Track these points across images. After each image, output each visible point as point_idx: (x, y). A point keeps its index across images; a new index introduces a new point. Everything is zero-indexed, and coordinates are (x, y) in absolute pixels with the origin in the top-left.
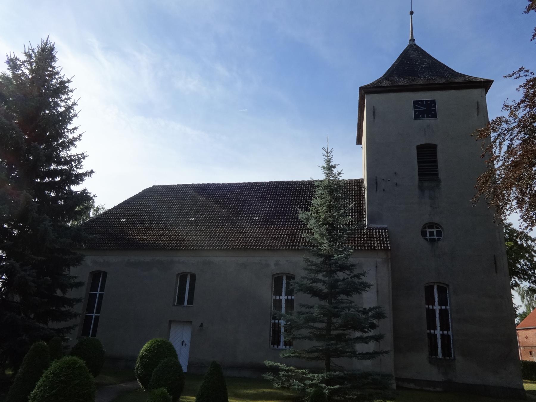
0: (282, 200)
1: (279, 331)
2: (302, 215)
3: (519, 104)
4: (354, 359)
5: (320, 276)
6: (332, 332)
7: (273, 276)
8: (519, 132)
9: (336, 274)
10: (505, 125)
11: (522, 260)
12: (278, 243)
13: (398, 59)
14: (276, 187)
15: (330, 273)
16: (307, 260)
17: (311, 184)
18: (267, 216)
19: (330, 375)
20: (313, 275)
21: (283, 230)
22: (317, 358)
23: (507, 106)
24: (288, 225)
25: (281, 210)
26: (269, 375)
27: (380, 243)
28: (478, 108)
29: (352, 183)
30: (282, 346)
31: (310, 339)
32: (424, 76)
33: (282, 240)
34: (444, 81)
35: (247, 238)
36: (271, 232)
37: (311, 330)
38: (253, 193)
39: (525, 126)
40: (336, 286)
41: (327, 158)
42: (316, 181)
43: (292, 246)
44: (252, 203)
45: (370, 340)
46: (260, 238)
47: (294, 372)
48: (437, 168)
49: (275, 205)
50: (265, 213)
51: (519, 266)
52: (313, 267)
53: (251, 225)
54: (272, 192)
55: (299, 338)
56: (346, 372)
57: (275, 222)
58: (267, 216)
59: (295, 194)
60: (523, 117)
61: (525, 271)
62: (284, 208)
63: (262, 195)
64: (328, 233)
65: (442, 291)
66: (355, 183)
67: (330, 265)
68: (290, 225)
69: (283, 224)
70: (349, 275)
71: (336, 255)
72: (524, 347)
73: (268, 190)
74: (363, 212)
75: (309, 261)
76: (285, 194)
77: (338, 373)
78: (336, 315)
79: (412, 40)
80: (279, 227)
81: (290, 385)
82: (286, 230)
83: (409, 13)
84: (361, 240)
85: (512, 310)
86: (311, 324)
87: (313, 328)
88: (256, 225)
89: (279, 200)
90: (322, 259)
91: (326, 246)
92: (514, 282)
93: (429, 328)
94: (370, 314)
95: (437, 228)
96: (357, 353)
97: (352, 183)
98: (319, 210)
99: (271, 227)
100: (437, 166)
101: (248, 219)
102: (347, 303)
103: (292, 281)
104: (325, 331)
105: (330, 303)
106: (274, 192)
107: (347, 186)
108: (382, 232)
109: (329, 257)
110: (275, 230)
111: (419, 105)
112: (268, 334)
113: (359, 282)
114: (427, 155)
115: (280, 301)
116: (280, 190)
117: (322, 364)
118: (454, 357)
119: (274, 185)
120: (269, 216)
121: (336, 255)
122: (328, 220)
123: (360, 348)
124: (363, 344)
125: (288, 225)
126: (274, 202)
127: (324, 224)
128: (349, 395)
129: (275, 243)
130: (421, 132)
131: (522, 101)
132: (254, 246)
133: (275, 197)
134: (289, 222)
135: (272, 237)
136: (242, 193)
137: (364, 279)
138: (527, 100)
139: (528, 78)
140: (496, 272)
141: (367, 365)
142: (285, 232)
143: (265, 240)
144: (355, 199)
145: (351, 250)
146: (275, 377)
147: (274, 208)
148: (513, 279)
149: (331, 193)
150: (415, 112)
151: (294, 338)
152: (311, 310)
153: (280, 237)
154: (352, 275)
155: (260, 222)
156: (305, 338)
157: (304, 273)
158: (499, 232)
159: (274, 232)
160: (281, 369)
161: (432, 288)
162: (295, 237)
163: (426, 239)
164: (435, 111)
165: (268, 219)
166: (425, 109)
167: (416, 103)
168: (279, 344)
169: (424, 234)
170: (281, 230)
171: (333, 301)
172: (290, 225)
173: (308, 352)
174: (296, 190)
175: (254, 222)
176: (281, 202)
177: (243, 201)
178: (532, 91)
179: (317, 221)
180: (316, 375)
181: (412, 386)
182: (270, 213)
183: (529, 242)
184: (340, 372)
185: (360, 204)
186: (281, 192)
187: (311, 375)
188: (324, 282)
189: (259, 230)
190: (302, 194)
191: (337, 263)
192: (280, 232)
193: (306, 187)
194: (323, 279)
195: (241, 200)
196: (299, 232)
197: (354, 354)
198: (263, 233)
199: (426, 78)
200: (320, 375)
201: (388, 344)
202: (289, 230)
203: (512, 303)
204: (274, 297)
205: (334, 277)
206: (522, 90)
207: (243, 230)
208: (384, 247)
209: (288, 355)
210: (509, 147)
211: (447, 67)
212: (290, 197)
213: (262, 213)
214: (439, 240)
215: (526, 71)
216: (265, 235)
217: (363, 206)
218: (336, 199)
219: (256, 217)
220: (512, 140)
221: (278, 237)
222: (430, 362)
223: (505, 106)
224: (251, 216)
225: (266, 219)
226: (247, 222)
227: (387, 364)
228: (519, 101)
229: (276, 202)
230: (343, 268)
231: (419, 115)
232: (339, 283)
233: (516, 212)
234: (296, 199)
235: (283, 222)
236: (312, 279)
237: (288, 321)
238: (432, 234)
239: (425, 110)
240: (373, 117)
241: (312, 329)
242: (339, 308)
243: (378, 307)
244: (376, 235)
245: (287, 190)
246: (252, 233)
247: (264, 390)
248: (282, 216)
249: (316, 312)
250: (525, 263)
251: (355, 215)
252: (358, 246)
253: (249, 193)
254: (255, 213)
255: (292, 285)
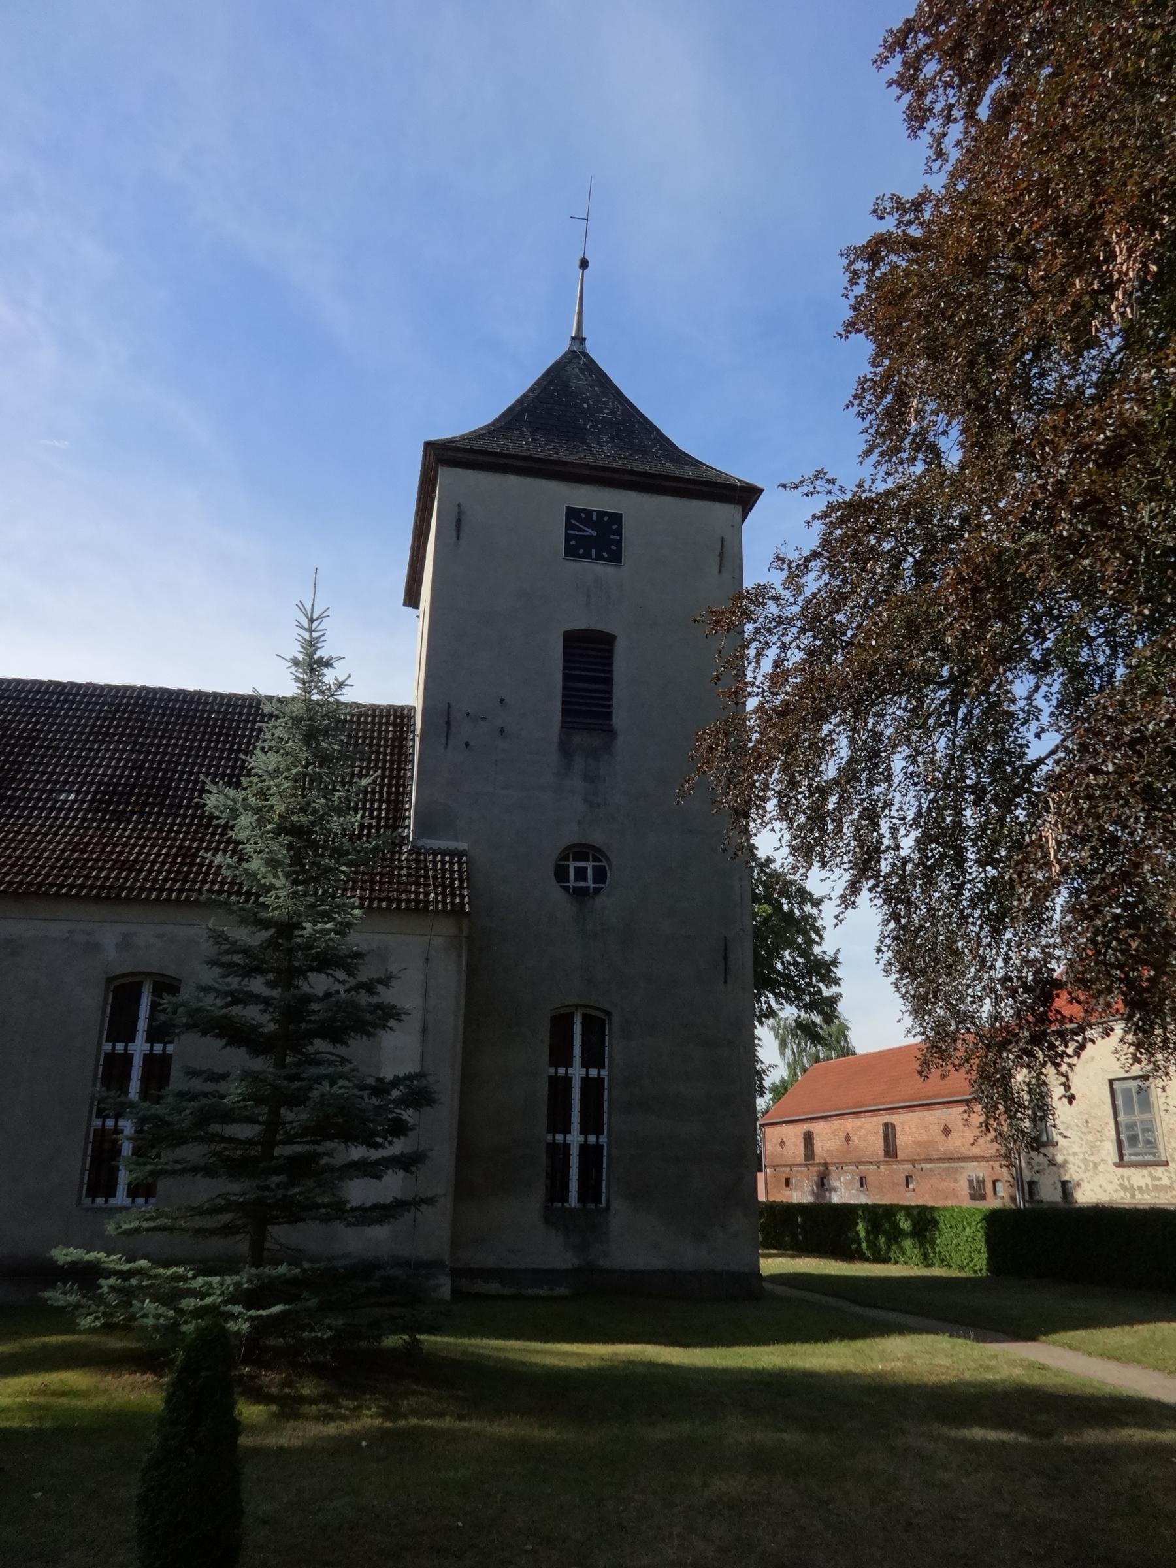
0: (159, 746)
1: (116, 1151)
2: (216, 799)
3: (807, 560)
4: (339, 1226)
5: (257, 985)
6: (278, 1151)
7: (109, 981)
8: (803, 630)
9: (306, 978)
10: (773, 608)
11: (787, 952)
12: (136, 880)
13: (537, 383)
14: (143, 705)
15: (287, 976)
16: (218, 937)
17: (250, 706)
18: (104, 793)
19: (259, 1277)
20: (234, 982)
21: (156, 839)
22: (227, 1230)
23: (783, 560)
24: (173, 824)
25: (155, 778)
26: (65, 1293)
27: (443, 893)
28: (721, 554)
29: (381, 716)
30: (121, 1198)
31: (209, 1171)
32: (600, 444)
33: (150, 871)
34: (647, 468)
35: (29, 858)
36: (115, 845)
37: (218, 1148)
38: (66, 716)
39: (816, 617)
40: (300, 1011)
41: (307, 635)
42: (270, 699)
43: (181, 891)
44: (57, 748)
45: (387, 1168)
46: (77, 860)
47: (150, 1277)
48: (611, 699)
49: (136, 761)
50: (100, 783)
51: (779, 966)
52: (237, 958)
53: (47, 818)
54: (129, 719)
55: (174, 1173)
56: (306, 1265)
57: (133, 813)
58: (104, 793)
59: (204, 733)
60: (814, 595)
61: (791, 978)
62: (166, 771)
63: (94, 726)
64: (292, 857)
65: (595, 1027)
66: (388, 716)
67: (290, 952)
68: (181, 825)
69: (155, 823)
70: (343, 982)
71: (308, 925)
72: (774, 1167)
73: (117, 711)
74: (403, 802)
75: (227, 939)
76: (173, 731)
77: (283, 1269)
78: (296, 1100)
79: (579, 339)
80: (143, 830)
81: (132, 1317)
82: (165, 839)
83: (578, 263)
84: (390, 883)
85: (752, 1076)
86: (216, 1128)
87: (222, 1139)
88: (65, 819)
89: (151, 745)
90: (266, 934)
91: (281, 895)
92: (764, 1007)
93: (552, 1129)
94: (395, 1093)
95: (596, 859)
96: (348, 1207)
97: (381, 716)
98: (269, 788)
99: (116, 829)
100: (610, 692)
101: (39, 799)
102: (330, 1063)
103: (166, 1000)
104: (259, 1148)
105: (280, 1064)
106: (137, 720)
107: (366, 723)
108: (452, 863)
109: (287, 928)
110: (129, 838)
111: (579, 520)
112: (75, 1164)
113: (370, 1004)
114: (588, 659)
115: (127, 1058)
116: (155, 714)
117: (241, 1245)
118: (608, 1201)
119: (139, 697)
120: (113, 793)
121: (308, 925)
122: (295, 818)
123: (359, 1192)
124: (367, 1180)
125: (173, 824)
126: (132, 751)
127: (281, 830)
128: (312, 1330)
129: (126, 879)
130: (577, 595)
131: (815, 555)
132: (52, 885)
133: (139, 735)
134: (177, 816)
135: (115, 861)
136: (24, 715)
137: (386, 996)
138: (826, 554)
139: (832, 499)
140: (725, 982)
141: (376, 1239)
142: (162, 847)
143: (92, 869)
144: (385, 761)
145: (356, 912)
146: (83, 1296)
147: (132, 769)
148: (763, 999)
149: (310, 737)
150: (568, 538)
151: (157, 1174)
152: (222, 1087)
153: (145, 862)
154: (352, 982)
155: (79, 810)
156: (195, 1169)
157: (209, 976)
158: (740, 879)
159: (125, 845)
160: (105, 1269)
161: (568, 1019)
162: (192, 864)
163: (566, 889)
164: (618, 543)
165: (109, 803)
166: (594, 533)
167: (572, 513)
168: (111, 1192)
169: (561, 874)
170: (147, 838)
171: (289, 1059)
172: (181, 825)
173: (200, 1212)
174: (208, 719)
175: (61, 809)
176: (156, 754)
177: (27, 738)
178: (839, 532)
179: (262, 822)
180: (216, 1280)
181: (494, 1287)
182: (117, 785)
183: (808, 908)
184: (290, 1264)
185: (399, 777)
186: (160, 723)
187: (200, 1280)
188: (267, 1002)
189: (74, 836)
190: (227, 735)
191: (312, 948)
192: (144, 846)
193: (241, 714)
194: (266, 992)
195: (20, 737)
196: (207, 850)
197: (340, 1211)
198: (88, 844)
199: (603, 451)
200: (228, 1280)
201: (437, 1177)
202: (175, 840)
203: (755, 1060)
204: (107, 1047)
205: (299, 987)
206: (819, 527)
207: (18, 833)
208: (453, 903)
209: (135, 1224)
210: (777, 663)
211: (658, 431)
212: (186, 739)
213: (91, 783)
214: (597, 891)
215: (829, 481)
216: (92, 852)
217: (404, 786)
218: (324, 759)
219: (69, 792)
220: (784, 647)
221: (136, 861)
222: (547, 1220)
223: (778, 558)
224: (52, 791)
225: (101, 801)
226: (34, 808)
227: (432, 1234)
228: (806, 553)
229: (140, 752)
230: (326, 961)
231: (576, 548)
232: (314, 1006)
233: (773, 830)
234: (207, 749)
235: (159, 814)
236: (230, 993)
237: (142, 1121)
238: (581, 874)
239: (595, 538)
240: (454, 534)
241: (220, 1142)
242: (302, 1079)
243: (419, 1076)
244: (434, 869)
245: (179, 716)
246: (50, 842)
247: (47, 1339)
248: (156, 796)
249: (233, 1092)
250: (793, 958)
251: (380, 810)
252: (380, 900)
253: (49, 716)
254: (66, 782)
255: (164, 1011)
